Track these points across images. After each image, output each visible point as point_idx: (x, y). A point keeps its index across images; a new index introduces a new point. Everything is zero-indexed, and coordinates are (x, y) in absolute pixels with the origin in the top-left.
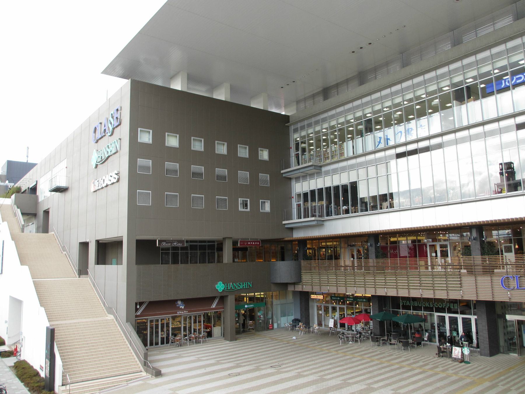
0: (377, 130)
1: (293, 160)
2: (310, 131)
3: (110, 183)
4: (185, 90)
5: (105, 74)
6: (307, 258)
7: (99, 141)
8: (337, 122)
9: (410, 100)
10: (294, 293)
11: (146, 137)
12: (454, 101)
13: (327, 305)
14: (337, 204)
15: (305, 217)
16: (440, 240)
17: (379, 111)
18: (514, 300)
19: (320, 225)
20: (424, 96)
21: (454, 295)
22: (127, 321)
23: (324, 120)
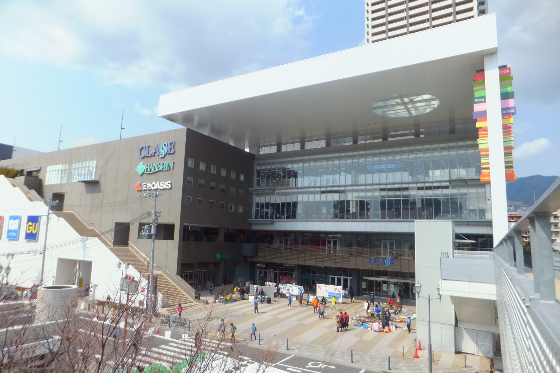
5: (531, 265)
7: (146, 158)
19: (272, 223)
22: (177, 274)
23: (269, 164)
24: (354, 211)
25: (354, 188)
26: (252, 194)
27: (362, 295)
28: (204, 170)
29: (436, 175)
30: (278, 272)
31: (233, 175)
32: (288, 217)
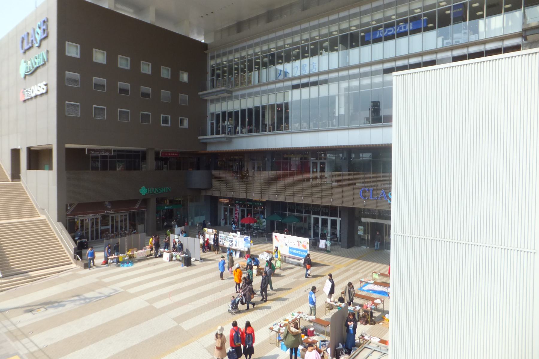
0: (278, 63)
1: (209, 83)
2: (225, 59)
3: (39, 93)
4: (112, 8)
6: (217, 168)
8: (247, 53)
9: (307, 40)
10: (206, 197)
11: (73, 51)
12: (340, 45)
13: (232, 207)
14: (243, 125)
15: (217, 134)
16: (321, 159)
17: (281, 47)
18: (367, 207)
19: (229, 141)
20: (394, 17)
21: (326, 202)
22: (59, 221)
23: (237, 50)
24: (342, 112)
25: (342, 74)
26: (206, 101)
27: (358, 246)
28: (105, 62)
29: (493, 27)
30: (246, 209)
31: (165, 73)
32: (250, 131)
